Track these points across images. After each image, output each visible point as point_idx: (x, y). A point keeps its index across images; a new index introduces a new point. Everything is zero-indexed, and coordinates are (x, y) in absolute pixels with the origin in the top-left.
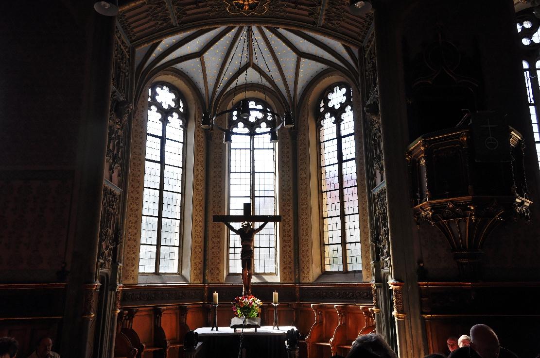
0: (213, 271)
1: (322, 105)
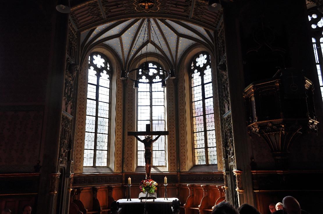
0: (128, 165)
1: (192, 65)
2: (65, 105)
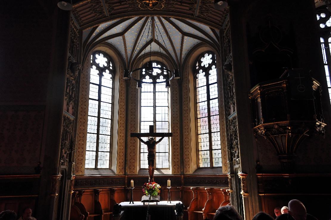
0: (130, 167)
1: (197, 65)
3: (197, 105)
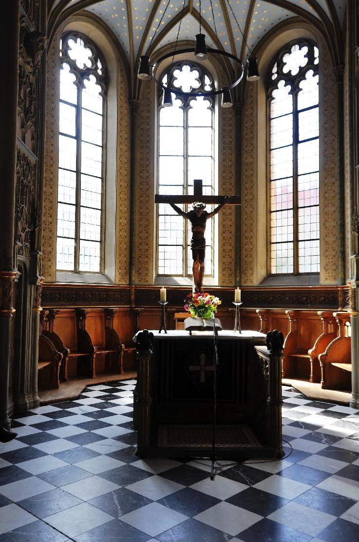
0: (140, 271)
1: (275, 70)
2: (20, 127)
3: (270, 153)
